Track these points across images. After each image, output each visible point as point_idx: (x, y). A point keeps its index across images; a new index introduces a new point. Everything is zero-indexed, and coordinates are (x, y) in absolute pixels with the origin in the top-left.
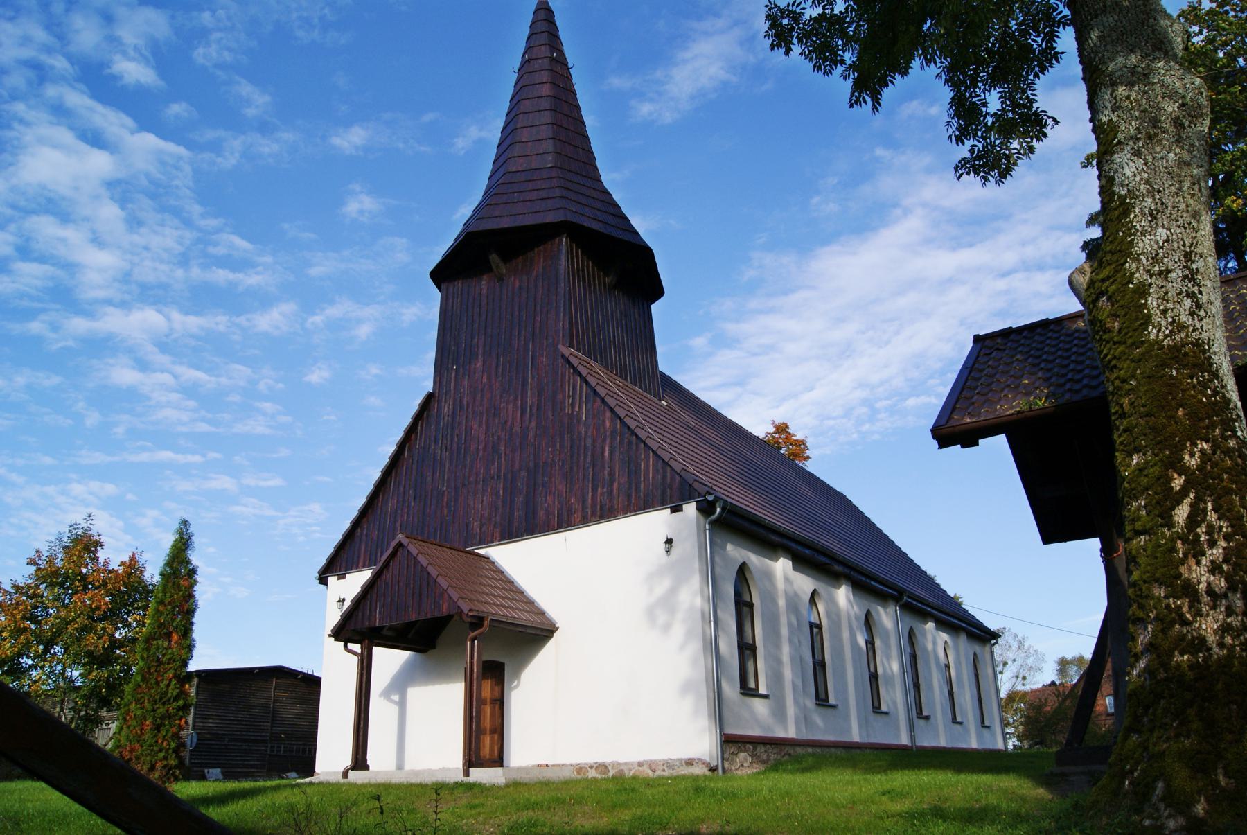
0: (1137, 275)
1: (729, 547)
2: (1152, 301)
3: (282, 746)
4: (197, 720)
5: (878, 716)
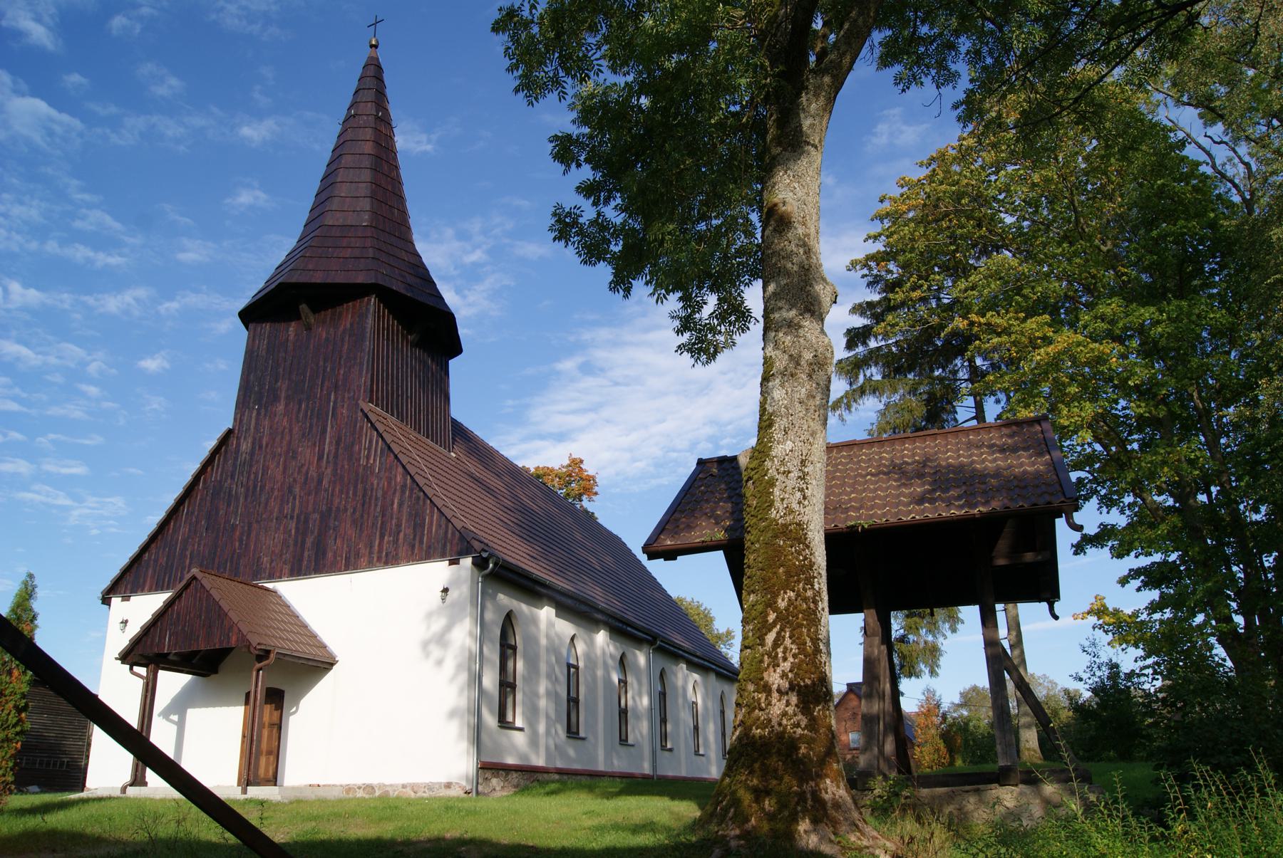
0: (770, 471)
1: (501, 597)
2: (777, 492)
5: (625, 748)
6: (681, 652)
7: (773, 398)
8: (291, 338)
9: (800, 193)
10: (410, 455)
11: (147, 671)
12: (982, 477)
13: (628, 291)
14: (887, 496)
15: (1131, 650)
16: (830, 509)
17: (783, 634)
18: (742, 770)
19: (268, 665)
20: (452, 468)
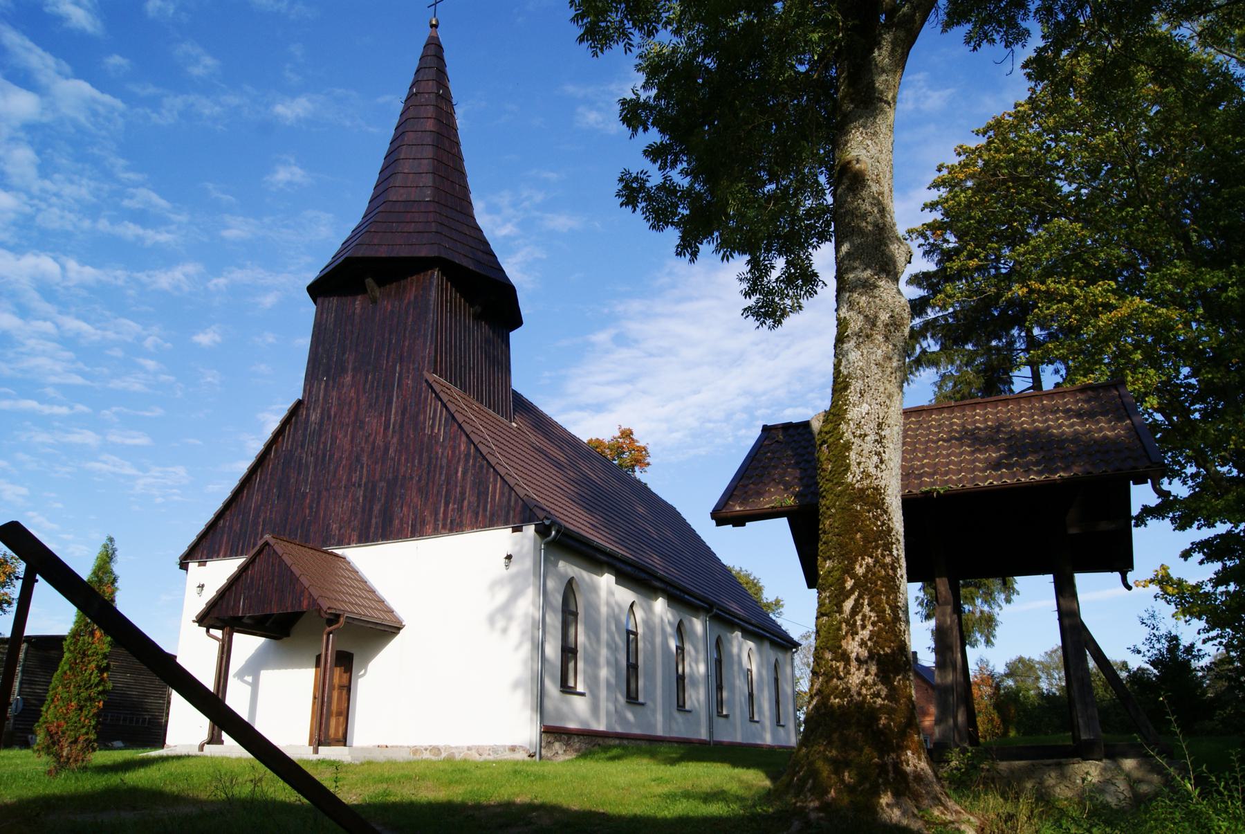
0: (846, 435)
1: (561, 564)
3: (110, 715)
4: (25, 686)
5: (682, 713)
6: (736, 620)
7: (848, 360)
8: (358, 311)
9: (873, 150)
10: (473, 424)
11: (223, 634)
12: (1060, 442)
13: (694, 255)
14: (961, 462)
15: (1195, 621)
16: (907, 475)
17: (861, 601)
18: (821, 741)
19: (338, 628)
20: (514, 437)
